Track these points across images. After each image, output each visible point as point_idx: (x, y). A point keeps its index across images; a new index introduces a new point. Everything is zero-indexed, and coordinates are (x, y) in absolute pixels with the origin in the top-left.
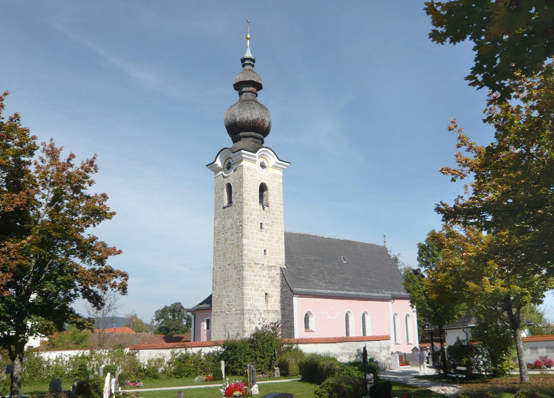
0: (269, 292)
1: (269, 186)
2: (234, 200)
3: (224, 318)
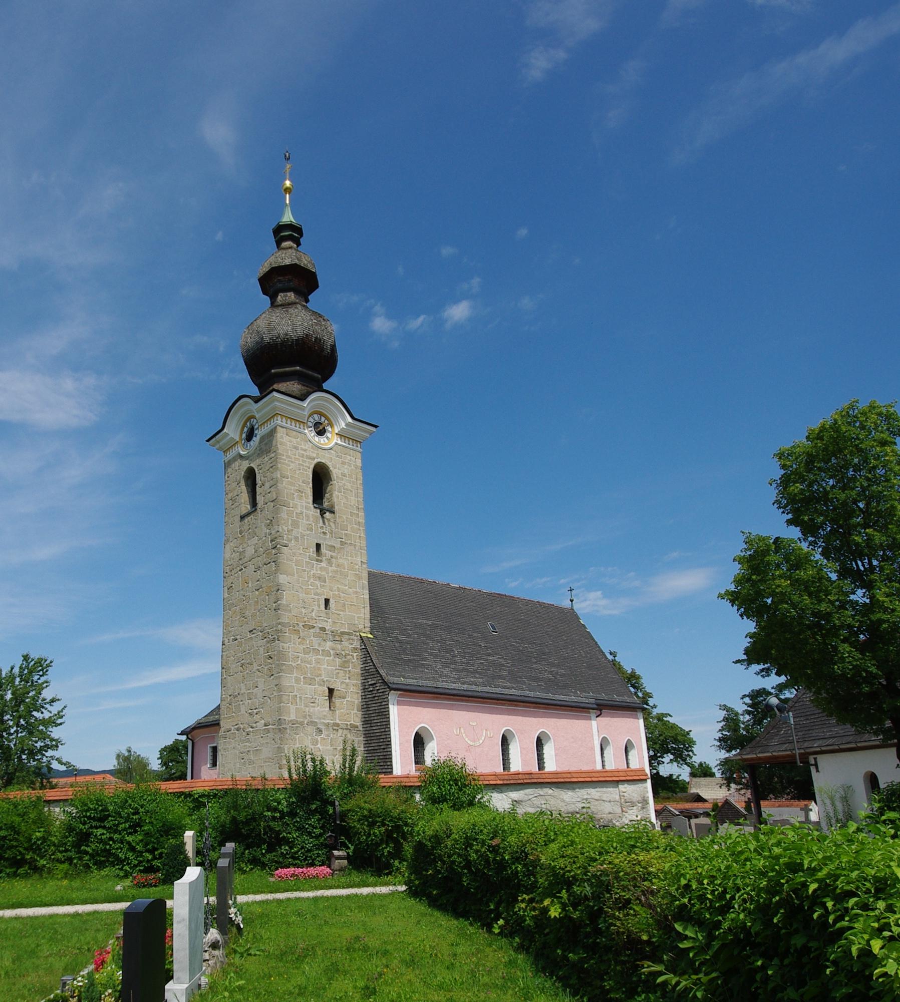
1: (335, 472)
2: (260, 499)
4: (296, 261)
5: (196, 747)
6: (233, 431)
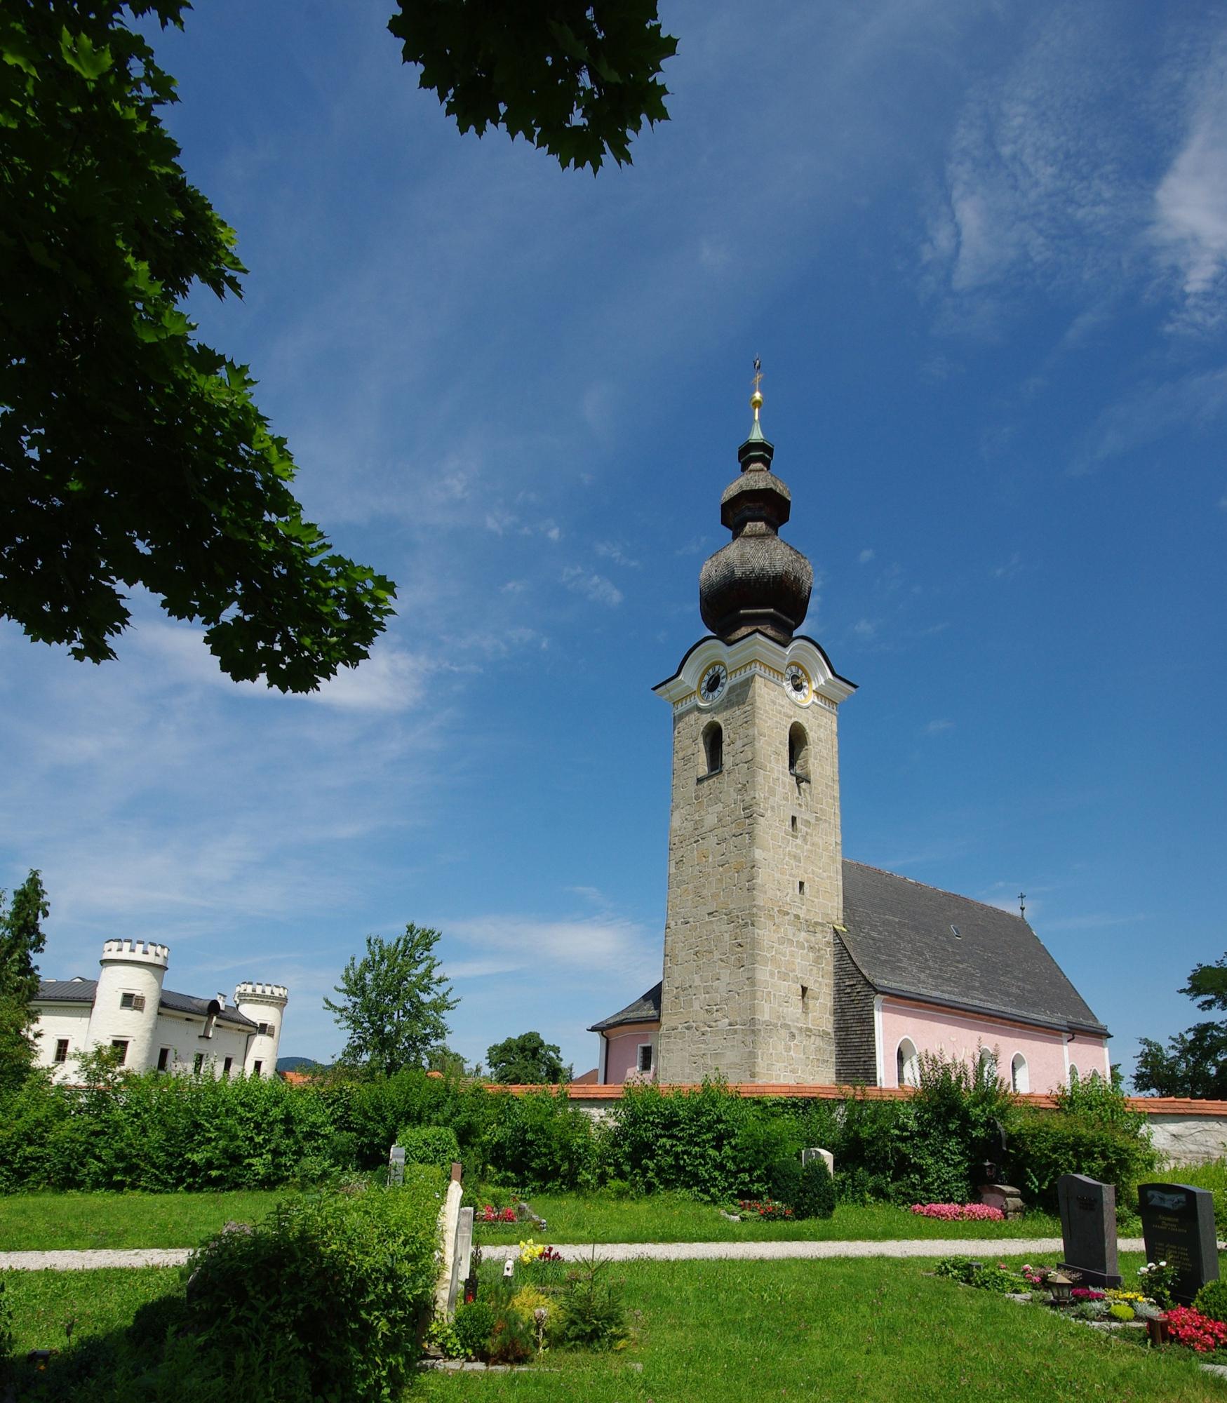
0: (810, 985)
1: (812, 735)
2: (727, 760)
3: (695, 1043)
4: (772, 486)
5: (611, 1046)
6: (690, 678)
